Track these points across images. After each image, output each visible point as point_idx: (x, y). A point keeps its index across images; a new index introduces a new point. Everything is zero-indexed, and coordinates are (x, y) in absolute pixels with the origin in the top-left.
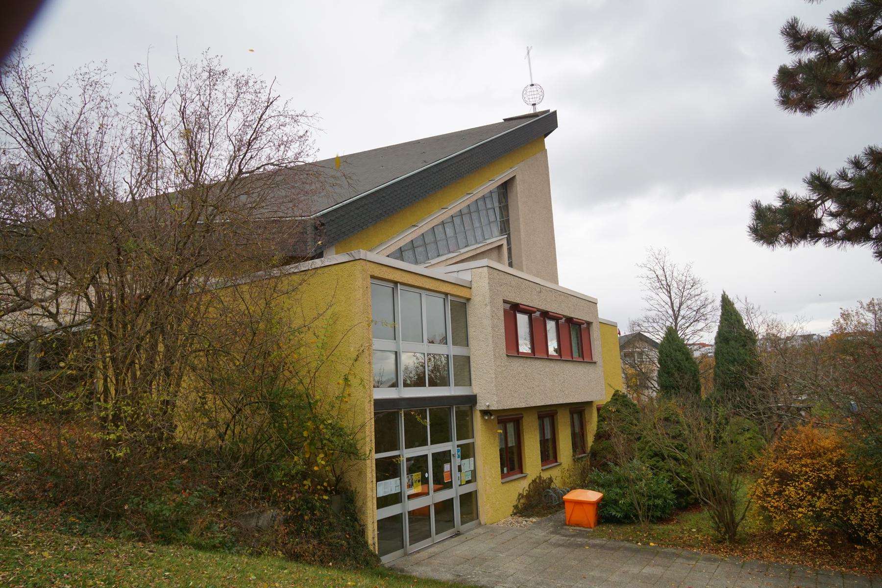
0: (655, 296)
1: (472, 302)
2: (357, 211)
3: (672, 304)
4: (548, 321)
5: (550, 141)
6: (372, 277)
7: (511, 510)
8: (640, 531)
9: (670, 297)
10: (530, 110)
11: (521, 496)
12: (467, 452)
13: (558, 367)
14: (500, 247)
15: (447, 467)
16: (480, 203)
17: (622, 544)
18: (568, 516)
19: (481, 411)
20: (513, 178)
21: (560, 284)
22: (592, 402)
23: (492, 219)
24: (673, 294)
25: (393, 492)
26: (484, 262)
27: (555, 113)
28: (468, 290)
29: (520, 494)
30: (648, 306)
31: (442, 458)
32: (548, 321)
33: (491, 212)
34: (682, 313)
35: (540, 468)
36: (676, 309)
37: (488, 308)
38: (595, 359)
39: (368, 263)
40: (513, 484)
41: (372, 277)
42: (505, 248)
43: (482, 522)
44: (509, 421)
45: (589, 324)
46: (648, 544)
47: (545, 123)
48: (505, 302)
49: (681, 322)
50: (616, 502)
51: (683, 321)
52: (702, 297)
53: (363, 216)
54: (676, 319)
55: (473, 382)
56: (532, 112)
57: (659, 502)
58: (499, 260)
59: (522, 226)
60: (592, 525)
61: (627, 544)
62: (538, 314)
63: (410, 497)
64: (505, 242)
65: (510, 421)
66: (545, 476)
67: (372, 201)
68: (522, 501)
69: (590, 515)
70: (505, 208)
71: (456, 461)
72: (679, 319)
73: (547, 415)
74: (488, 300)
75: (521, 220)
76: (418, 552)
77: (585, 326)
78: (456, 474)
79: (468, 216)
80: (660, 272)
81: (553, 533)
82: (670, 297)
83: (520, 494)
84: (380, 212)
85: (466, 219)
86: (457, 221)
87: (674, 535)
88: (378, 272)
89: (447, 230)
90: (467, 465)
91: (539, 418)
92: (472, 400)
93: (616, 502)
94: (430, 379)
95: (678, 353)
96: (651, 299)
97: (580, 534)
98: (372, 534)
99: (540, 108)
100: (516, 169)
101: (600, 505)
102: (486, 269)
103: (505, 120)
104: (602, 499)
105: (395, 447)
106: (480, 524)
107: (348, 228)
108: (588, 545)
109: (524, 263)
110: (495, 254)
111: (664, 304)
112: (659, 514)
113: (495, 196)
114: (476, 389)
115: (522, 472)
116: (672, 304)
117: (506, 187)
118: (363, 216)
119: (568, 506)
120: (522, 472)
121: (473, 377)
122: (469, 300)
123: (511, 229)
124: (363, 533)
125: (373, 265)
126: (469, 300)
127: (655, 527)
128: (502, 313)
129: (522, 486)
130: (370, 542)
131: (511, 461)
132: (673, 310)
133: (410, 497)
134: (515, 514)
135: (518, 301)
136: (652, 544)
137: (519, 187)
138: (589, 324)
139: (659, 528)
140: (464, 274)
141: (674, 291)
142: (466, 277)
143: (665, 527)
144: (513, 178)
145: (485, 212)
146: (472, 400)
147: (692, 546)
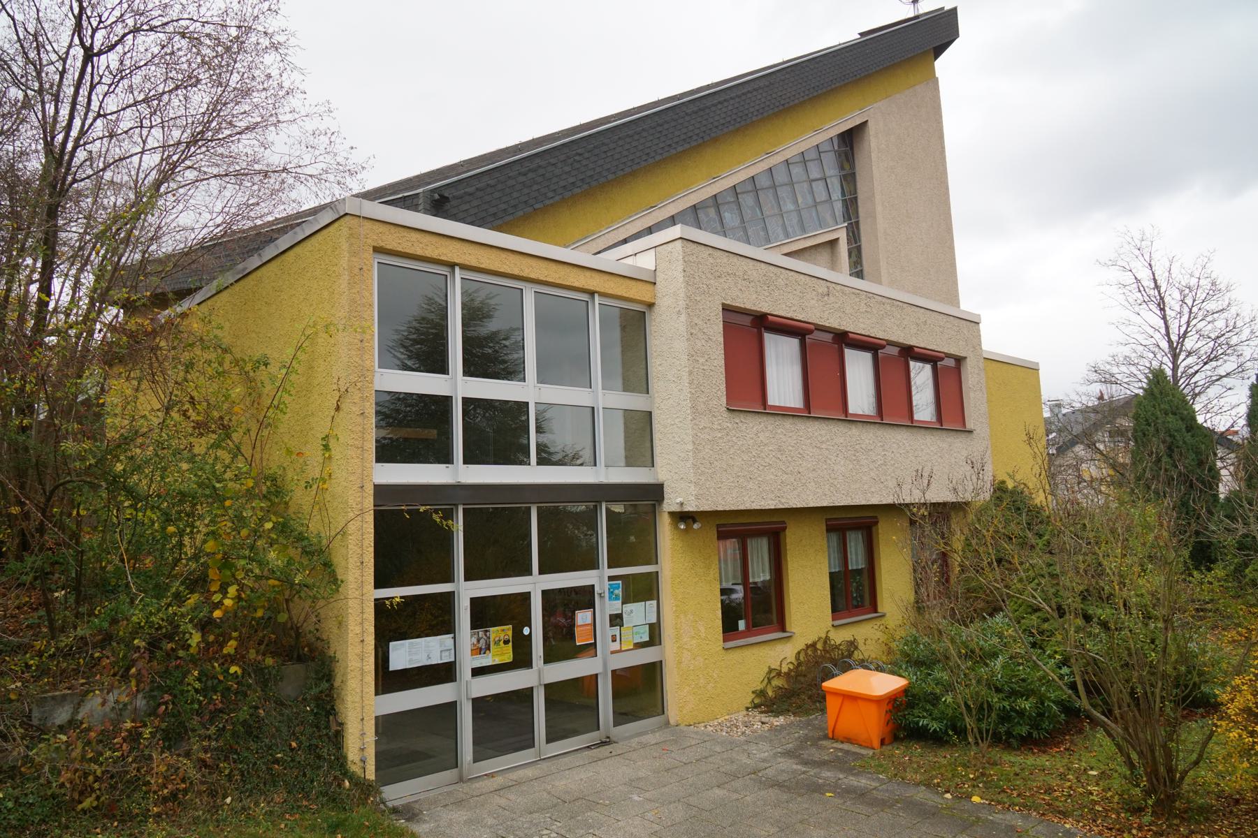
0: (1134, 318)
1: (656, 308)
2: (522, 179)
3: (1167, 328)
4: (912, 364)
5: (943, 65)
6: (378, 250)
7: (748, 699)
8: (965, 766)
9: (1164, 318)
10: (907, 12)
11: (773, 674)
12: (643, 589)
13: (869, 437)
14: (833, 243)
15: (583, 617)
16: (797, 171)
17: (911, 792)
18: (831, 724)
19: (672, 514)
20: (864, 124)
21: (962, 307)
22: (967, 503)
23: (821, 194)
24: (1168, 312)
25: (435, 660)
26: (676, 231)
27: (954, 12)
28: (649, 287)
29: (771, 670)
30: (1122, 338)
31: (563, 605)
32: (912, 364)
33: (819, 187)
34: (1189, 344)
35: (830, 622)
36: (1174, 338)
37: (683, 318)
38: (969, 426)
39: (368, 224)
40: (755, 650)
41: (378, 250)
42: (843, 247)
43: (672, 722)
44: (753, 534)
45: (959, 360)
46: (969, 797)
47: (937, 32)
48: (727, 309)
49: (1185, 362)
50: (934, 699)
51: (1190, 360)
52: (1233, 310)
53: (536, 187)
54: (1175, 357)
55: (657, 459)
56: (911, 15)
57: (1026, 705)
58: (833, 265)
59: (879, 208)
60: (876, 743)
61: (921, 794)
62: (894, 351)
63: (477, 672)
64: (842, 235)
65: (759, 533)
66: (839, 637)
67: (553, 161)
68: (776, 682)
69: (872, 724)
70: (849, 179)
71: (608, 606)
72: (1182, 357)
73: (852, 525)
74: (682, 304)
75: (878, 197)
76: (492, 775)
77: (950, 363)
78: (605, 630)
79: (770, 193)
80: (1145, 275)
81: (788, 754)
82: (1164, 318)
83: (771, 670)
84: (572, 180)
85: (767, 198)
86: (747, 200)
87: (1039, 780)
88: (392, 241)
89: (727, 216)
90: (638, 615)
91: (830, 529)
92: (655, 492)
93: (934, 699)
94: (541, 448)
95: (1170, 418)
96: (1129, 323)
97: (838, 763)
98: (360, 746)
99: (925, 7)
100: (881, 114)
101: (898, 704)
102: (679, 244)
103: (862, 34)
104: (905, 691)
105: (449, 578)
106: (667, 723)
107: (503, 206)
108: (837, 789)
109: (884, 272)
110: (825, 255)
111: (1151, 331)
112: (1024, 730)
113: (830, 160)
114: (662, 472)
115: (783, 629)
116: (1167, 328)
117: (850, 139)
118: (536, 187)
119: (832, 704)
120: (783, 629)
121: (657, 450)
122: (651, 306)
123: (861, 214)
124: (337, 739)
125: (382, 228)
126: (651, 306)
127: (1008, 757)
128: (719, 327)
129: (778, 654)
130: (352, 754)
131: (752, 610)
132: (1170, 342)
133: (477, 672)
134: (756, 706)
135: (764, 307)
136: (976, 799)
137: (875, 147)
138: (959, 360)
139: (1013, 761)
140: (640, 258)
141: (1173, 300)
142: (646, 262)
143: (1020, 759)
144: (864, 124)
145: (806, 185)
146: (655, 492)
147: (1065, 814)
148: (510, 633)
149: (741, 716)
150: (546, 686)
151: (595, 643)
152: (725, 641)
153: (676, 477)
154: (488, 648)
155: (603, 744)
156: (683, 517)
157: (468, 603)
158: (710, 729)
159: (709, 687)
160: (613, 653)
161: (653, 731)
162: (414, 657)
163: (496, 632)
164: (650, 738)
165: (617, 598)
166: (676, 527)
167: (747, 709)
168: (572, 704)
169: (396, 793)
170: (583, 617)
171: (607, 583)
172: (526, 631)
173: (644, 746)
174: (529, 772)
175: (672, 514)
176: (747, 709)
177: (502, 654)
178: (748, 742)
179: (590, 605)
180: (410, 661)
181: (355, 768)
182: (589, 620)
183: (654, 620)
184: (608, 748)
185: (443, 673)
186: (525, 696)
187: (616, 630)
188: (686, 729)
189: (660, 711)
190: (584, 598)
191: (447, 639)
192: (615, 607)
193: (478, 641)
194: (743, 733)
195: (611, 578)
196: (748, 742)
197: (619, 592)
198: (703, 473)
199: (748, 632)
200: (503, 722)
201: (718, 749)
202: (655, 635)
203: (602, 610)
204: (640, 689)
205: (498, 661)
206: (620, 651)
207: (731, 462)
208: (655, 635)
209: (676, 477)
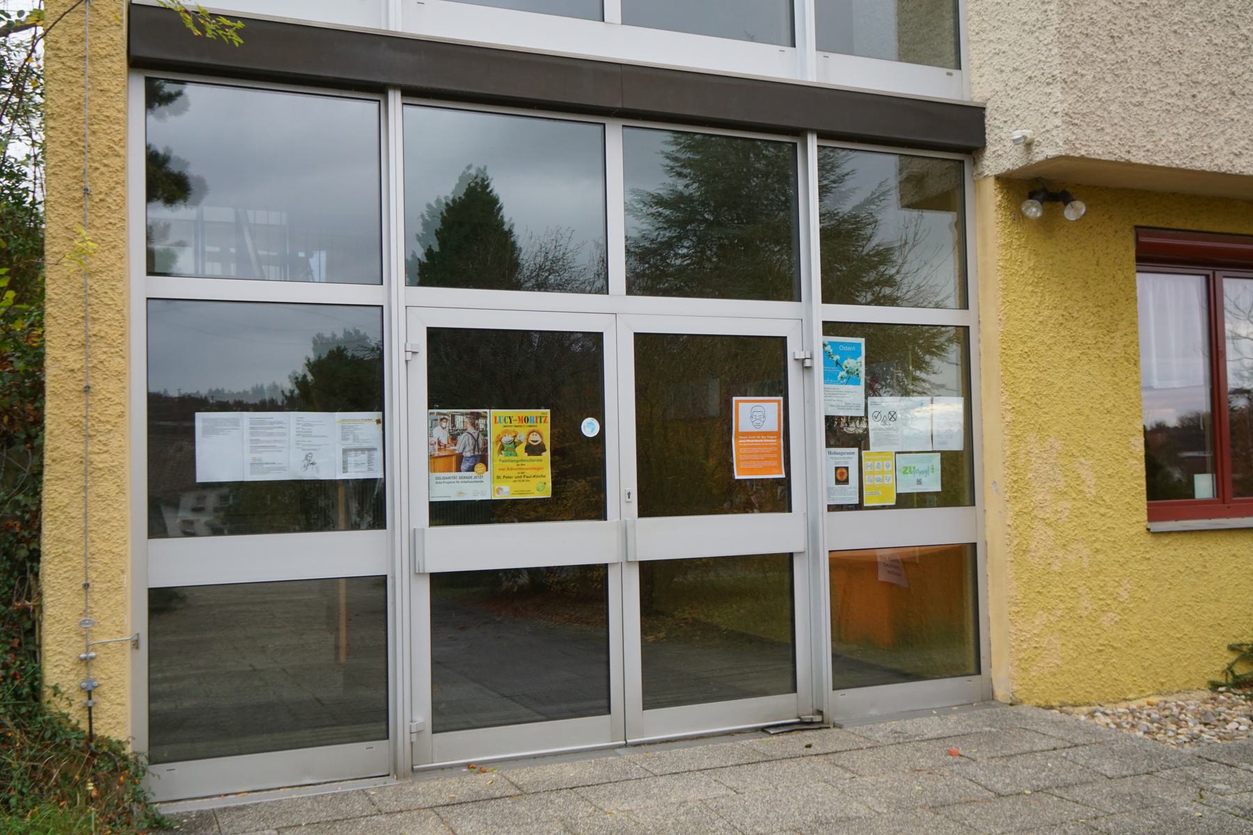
7: (1218, 663)
15: (752, 414)
43: (1001, 693)
71: (817, 394)
94: (838, 235)
106: (989, 698)
133: (444, 513)
148: (546, 429)
149: (1197, 699)
150: (643, 565)
151: (786, 483)
152: (1152, 516)
153: (1016, 79)
154: (482, 458)
155: (803, 725)
156: (1045, 190)
157: (421, 343)
158: (1101, 720)
159: (1105, 620)
160: (832, 508)
161: (944, 712)
162: (266, 457)
163: (500, 422)
164: (932, 726)
165: (851, 377)
166: (1019, 217)
167: (1214, 686)
168: (717, 627)
169: (188, 785)
170: (752, 414)
171: (819, 338)
172: (589, 428)
173: (901, 740)
174: (570, 771)
175: (1007, 181)
176: (1214, 686)
177: (522, 477)
178: (1202, 760)
179: (778, 387)
180: (256, 464)
181: (65, 705)
182: (772, 422)
183: (957, 445)
184: (810, 736)
185: (366, 503)
186: (588, 585)
187: (848, 457)
188: (1035, 712)
189: (972, 669)
190: (761, 365)
191: (363, 421)
192: (848, 399)
193: (454, 438)
194: (1194, 738)
195: (830, 328)
196: (1202, 760)
197: (858, 363)
198: (1088, 60)
199: (1221, 503)
200: (522, 635)
201: (1108, 768)
202: (957, 479)
203: (809, 401)
204: (917, 615)
205: (507, 492)
206: (859, 507)
207: (1173, 42)
208: (957, 479)
209: (1016, 79)
